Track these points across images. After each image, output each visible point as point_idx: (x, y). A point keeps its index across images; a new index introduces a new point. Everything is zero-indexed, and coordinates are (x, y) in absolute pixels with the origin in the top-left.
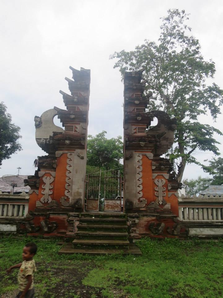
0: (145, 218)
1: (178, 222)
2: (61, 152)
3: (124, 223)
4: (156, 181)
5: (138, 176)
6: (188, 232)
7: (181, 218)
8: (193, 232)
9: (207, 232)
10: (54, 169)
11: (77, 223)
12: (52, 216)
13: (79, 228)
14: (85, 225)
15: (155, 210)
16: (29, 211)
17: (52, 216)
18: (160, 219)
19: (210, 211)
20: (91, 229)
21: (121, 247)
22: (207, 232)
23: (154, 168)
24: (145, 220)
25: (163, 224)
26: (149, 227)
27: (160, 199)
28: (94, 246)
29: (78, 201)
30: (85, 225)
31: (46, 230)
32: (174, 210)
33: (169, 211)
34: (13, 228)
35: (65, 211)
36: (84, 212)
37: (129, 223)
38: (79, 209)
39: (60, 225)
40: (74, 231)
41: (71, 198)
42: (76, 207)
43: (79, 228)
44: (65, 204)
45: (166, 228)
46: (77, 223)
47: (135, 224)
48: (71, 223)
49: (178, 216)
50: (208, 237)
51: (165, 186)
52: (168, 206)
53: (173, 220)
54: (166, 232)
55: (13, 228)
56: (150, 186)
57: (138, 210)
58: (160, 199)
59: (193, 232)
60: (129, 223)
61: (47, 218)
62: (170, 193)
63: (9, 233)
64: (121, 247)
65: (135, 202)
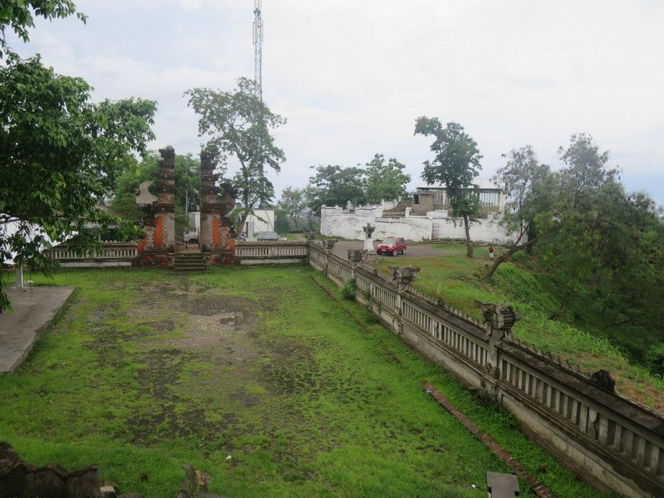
0: (214, 255)
1: (234, 257)
2: (158, 215)
3: (202, 258)
4: (221, 233)
5: (210, 230)
6: (239, 262)
7: (236, 254)
8: (243, 262)
9: (251, 262)
10: (155, 226)
11: (174, 259)
12: (156, 256)
13: (175, 262)
14: (178, 260)
15: (220, 250)
16: (138, 253)
17: (156, 256)
18: (223, 255)
19: (125, 251)
20: (182, 262)
21: (201, 270)
22: (251, 262)
23: (220, 224)
24: (213, 256)
25: (224, 258)
26: (216, 260)
27: (224, 243)
28: (186, 270)
29: (172, 246)
30: (178, 260)
31: (153, 263)
32: (232, 250)
33: (228, 251)
34: (130, 264)
35: (165, 252)
36: (176, 253)
37: (205, 258)
38: (173, 251)
39: (162, 260)
40: (527, 150)
41: (167, 245)
42: (171, 249)
43: (175, 262)
44: (163, 248)
45: (226, 260)
46: (174, 259)
47: (208, 259)
48: (170, 259)
49: (235, 253)
50: (252, 265)
51: (228, 235)
52: (228, 247)
53: (231, 256)
54: (227, 263)
55: (130, 264)
56: (217, 236)
57: (209, 251)
58: (224, 243)
59: (243, 262)
60: (205, 258)
61: (153, 256)
62: (230, 240)
63: (128, 267)
64: (201, 270)
65: (208, 246)
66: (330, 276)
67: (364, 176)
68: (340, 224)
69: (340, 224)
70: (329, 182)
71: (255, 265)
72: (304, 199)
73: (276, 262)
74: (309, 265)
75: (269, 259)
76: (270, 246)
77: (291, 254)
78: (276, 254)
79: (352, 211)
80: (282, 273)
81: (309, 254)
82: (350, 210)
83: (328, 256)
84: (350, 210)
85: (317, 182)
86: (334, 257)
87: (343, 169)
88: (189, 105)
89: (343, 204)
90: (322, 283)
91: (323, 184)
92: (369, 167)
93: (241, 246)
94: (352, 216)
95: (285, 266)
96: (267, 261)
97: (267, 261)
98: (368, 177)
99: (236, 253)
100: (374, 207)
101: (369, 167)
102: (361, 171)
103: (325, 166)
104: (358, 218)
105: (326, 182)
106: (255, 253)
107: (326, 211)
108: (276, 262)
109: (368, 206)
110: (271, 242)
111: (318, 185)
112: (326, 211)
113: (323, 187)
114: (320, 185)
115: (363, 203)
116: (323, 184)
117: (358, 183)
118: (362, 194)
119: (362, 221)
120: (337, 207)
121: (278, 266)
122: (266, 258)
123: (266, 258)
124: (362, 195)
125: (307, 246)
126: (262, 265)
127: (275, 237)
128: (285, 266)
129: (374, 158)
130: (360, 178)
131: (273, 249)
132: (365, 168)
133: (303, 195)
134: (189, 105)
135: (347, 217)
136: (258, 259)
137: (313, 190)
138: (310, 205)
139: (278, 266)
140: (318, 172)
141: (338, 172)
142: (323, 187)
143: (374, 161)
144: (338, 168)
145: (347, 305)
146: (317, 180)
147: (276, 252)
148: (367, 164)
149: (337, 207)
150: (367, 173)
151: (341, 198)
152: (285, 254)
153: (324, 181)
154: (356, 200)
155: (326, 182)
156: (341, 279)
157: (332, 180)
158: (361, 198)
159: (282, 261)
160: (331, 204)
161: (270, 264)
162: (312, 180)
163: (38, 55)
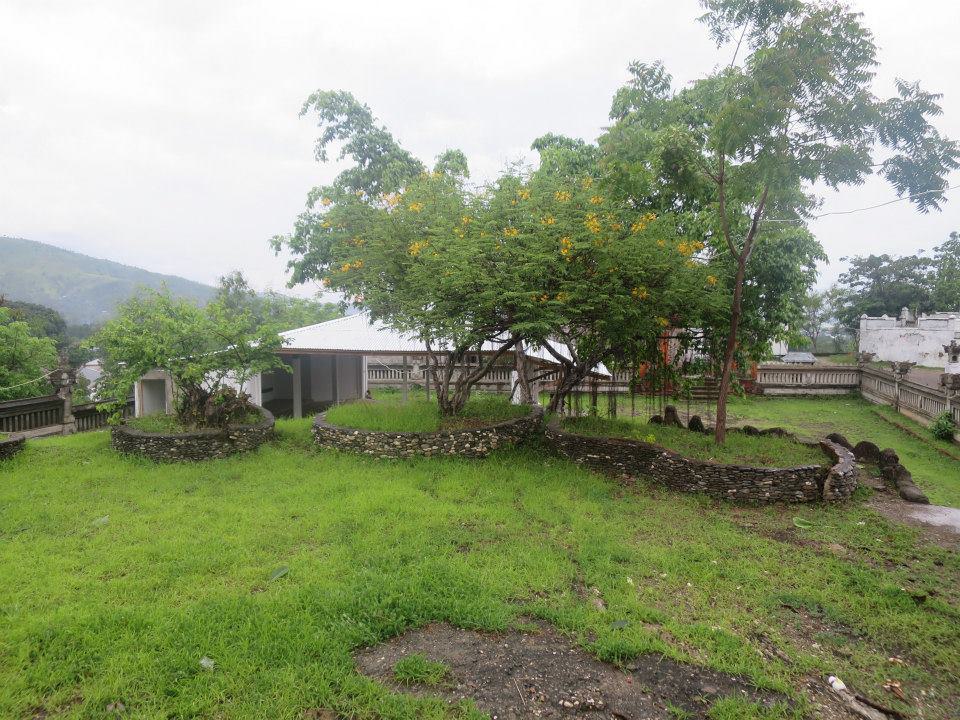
6: (763, 391)
7: (758, 381)
50: (779, 395)
66: (903, 411)
67: (930, 268)
68: (887, 340)
69: (887, 340)
70: (871, 280)
71: (784, 395)
72: (827, 306)
73: (813, 392)
74: (862, 397)
75: (804, 387)
76: (803, 370)
77: (834, 383)
78: (813, 382)
79: (910, 323)
80: (826, 406)
81: (860, 382)
82: (907, 322)
83: (900, 385)
84: (907, 322)
85: (851, 280)
86: (909, 385)
87: (895, 259)
88: (304, 112)
89: (896, 312)
90: (892, 420)
91: (861, 284)
92: (939, 253)
93: (766, 371)
94: (911, 330)
95: (828, 398)
96: (800, 391)
97: (800, 391)
98: (936, 270)
99: (759, 380)
100: (952, 316)
101: (939, 253)
102: (926, 262)
103: (866, 256)
104: (921, 332)
105: (866, 280)
106: (787, 380)
107: (867, 323)
108: (813, 392)
109: (939, 315)
110: (806, 366)
111: (852, 286)
112: (867, 323)
113: (860, 288)
114: (856, 284)
115: (929, 310)
116: (861, 284)
117: (918, 279)
118: (927, 296)
119: (930, 338)
120: (885, 316)
121: (816, 397)
122: (799, 387)
123: (799, 387)
124: (927, 297)
125: (859, 372)
126: (794, 396)
127: (811, 360)
128: (828, 398)
129: (949, 239)
130: (923, 272)
131: (809, 375)
132: (931, 255)
133: (825, 300)
134: (304, 112)
135: (903, 331)
136: (787, 387)
137: (842, 292)
138: (839, 315)
139: (816, 397)
140: (852, 266)
141: (885, 264)
142: (860, 288)
143: (948, 243)
144: (886, 258)
145: (943, 445)
146: (851, 278)
147: (813, 379)
148: (936, 249)
149: (885, 316)
150: (934, 264)
151: (893, 303)
152: (826, 382)
153: (862, 278)
154: (917, 305)
155: (866, 280)
156: (926, 415)
157: (877, 277)
158: (927, 303)
159: (821, 392)
160: (875, 312)
161: (804, 395)
162: (843, 278)
163: (329, 104)
